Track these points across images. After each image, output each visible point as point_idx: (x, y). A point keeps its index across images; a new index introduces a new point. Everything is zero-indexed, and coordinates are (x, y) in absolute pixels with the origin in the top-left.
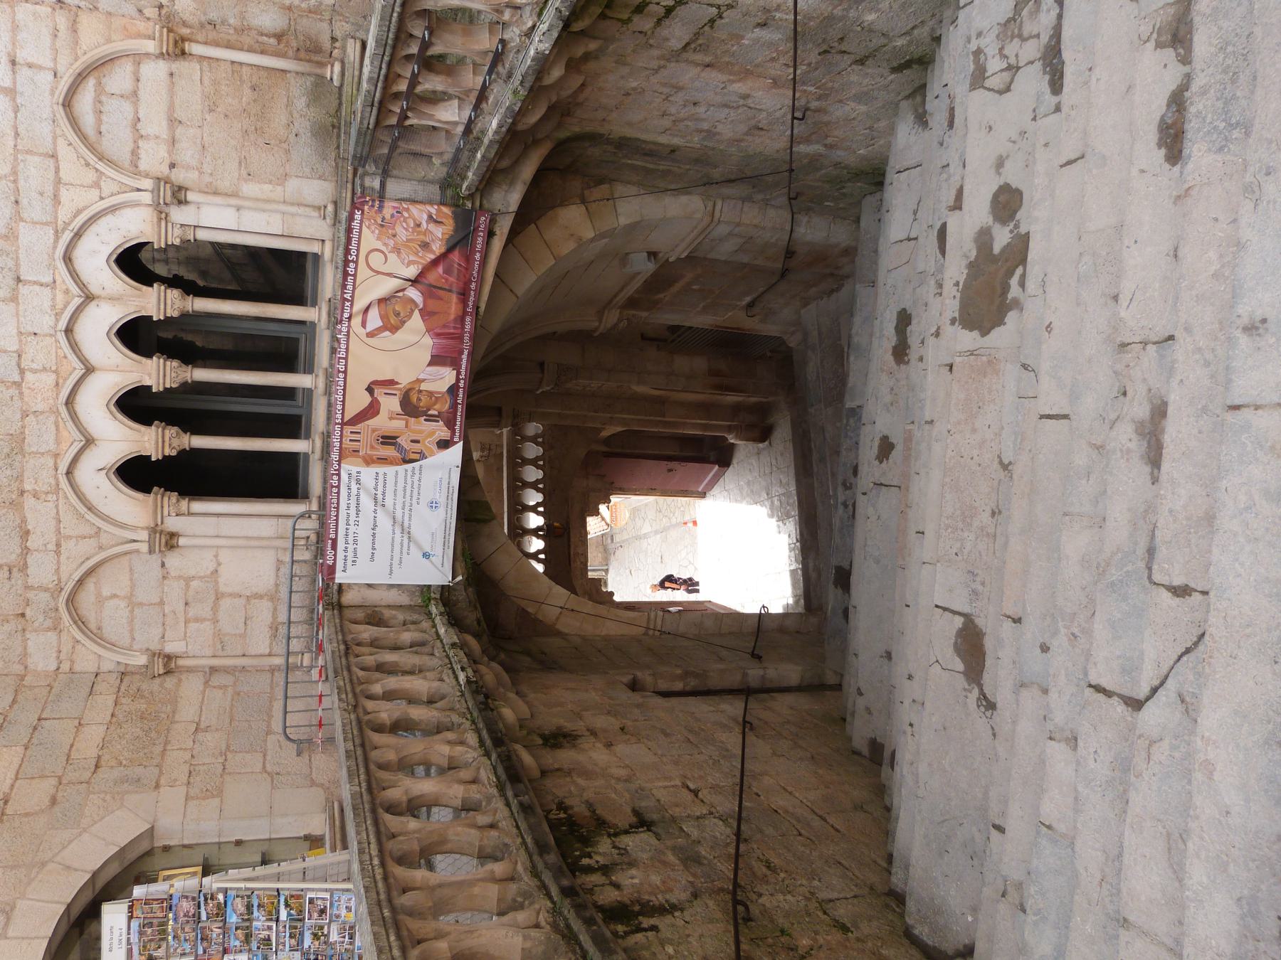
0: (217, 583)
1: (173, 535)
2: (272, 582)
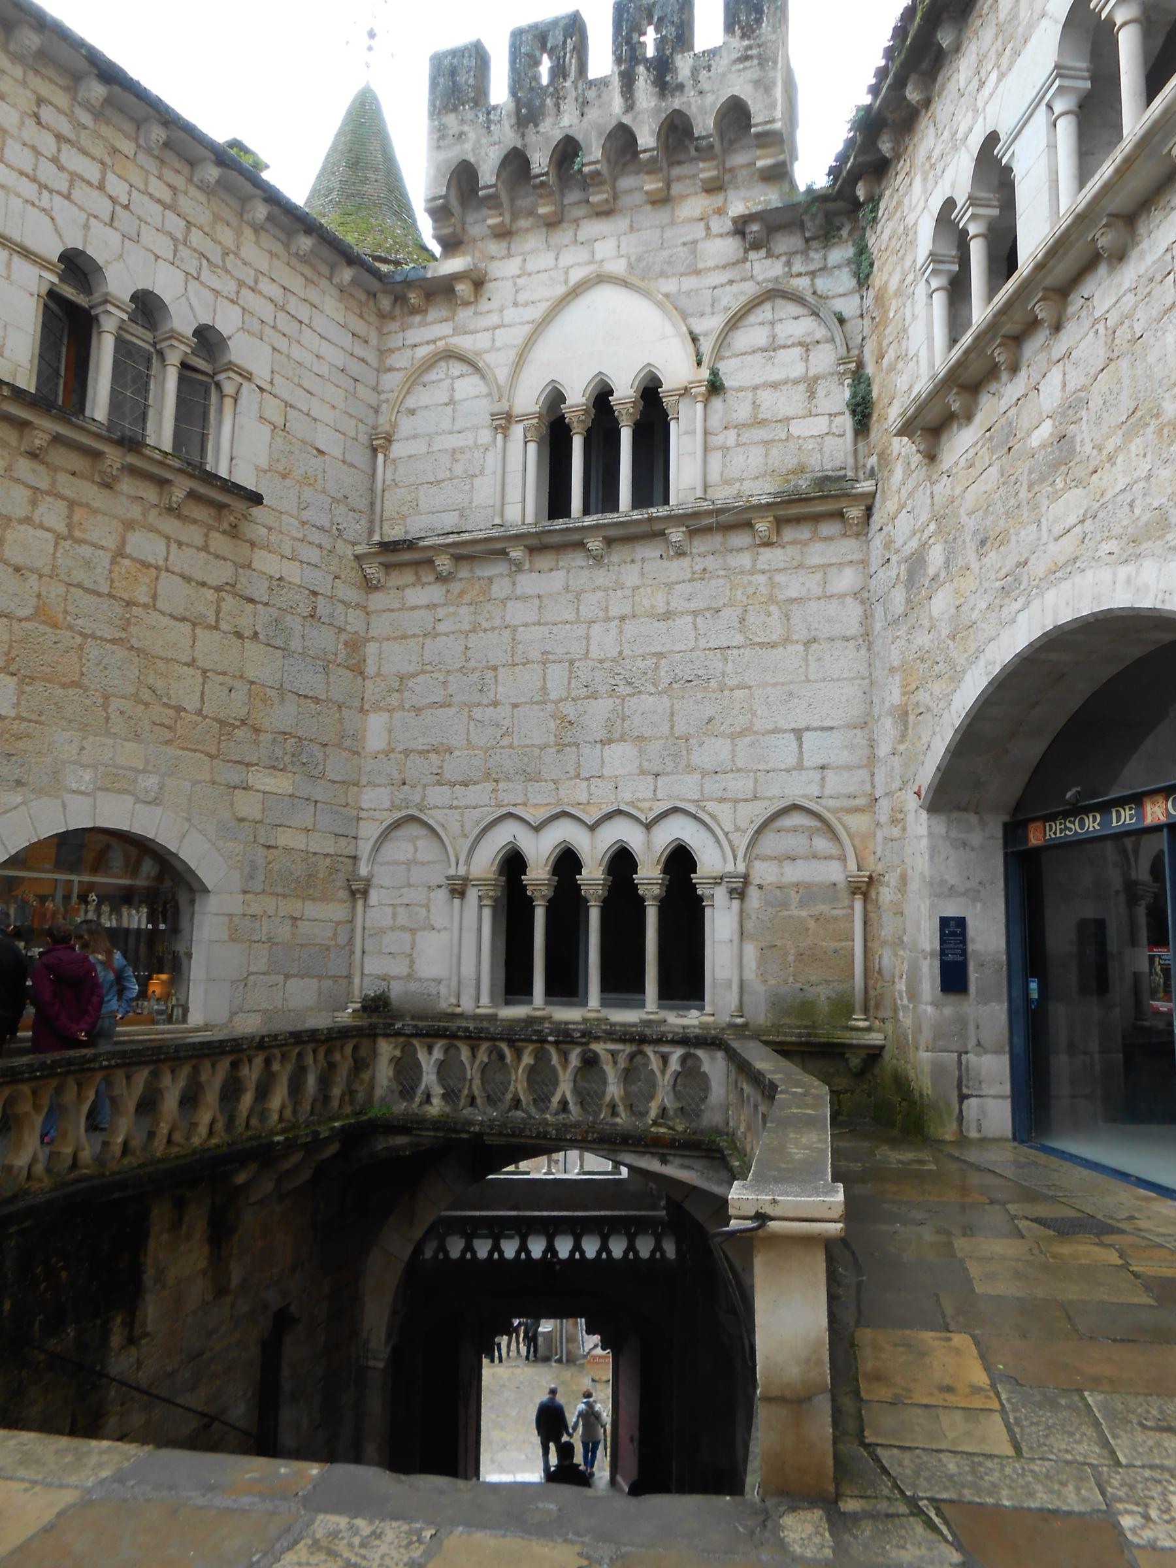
0: (424, 929)
1: (462, 894)
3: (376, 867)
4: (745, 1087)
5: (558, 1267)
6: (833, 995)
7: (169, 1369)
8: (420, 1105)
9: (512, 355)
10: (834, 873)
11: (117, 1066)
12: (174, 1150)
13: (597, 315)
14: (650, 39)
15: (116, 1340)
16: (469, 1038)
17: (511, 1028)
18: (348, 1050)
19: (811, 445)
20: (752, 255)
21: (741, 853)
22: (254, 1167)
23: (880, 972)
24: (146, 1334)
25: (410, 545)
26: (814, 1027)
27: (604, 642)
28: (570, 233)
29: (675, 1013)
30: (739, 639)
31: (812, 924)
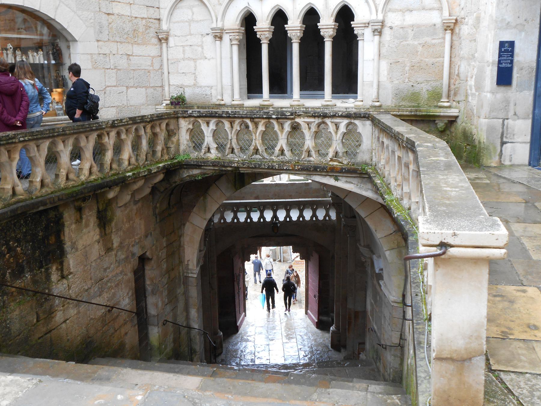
0: (201, 59)
1: (221, 38)
2: (203, 84)
3: (171, 25)
4: (385, 140)
5: (279, 225)
6: (430, 88)
7: (86, 288)
8: (205, 153)
11: (29, 140)
12: (71, 184)
15: (54, 277)
16: (229, 117)
17: (252, 112)
18: (164, 126)
21: (380, 8)
22: (117, 189)
23: (458, 75)
24: (71, 273)
26: (418, 107)
29: (340, 101)
31: (420, 49)
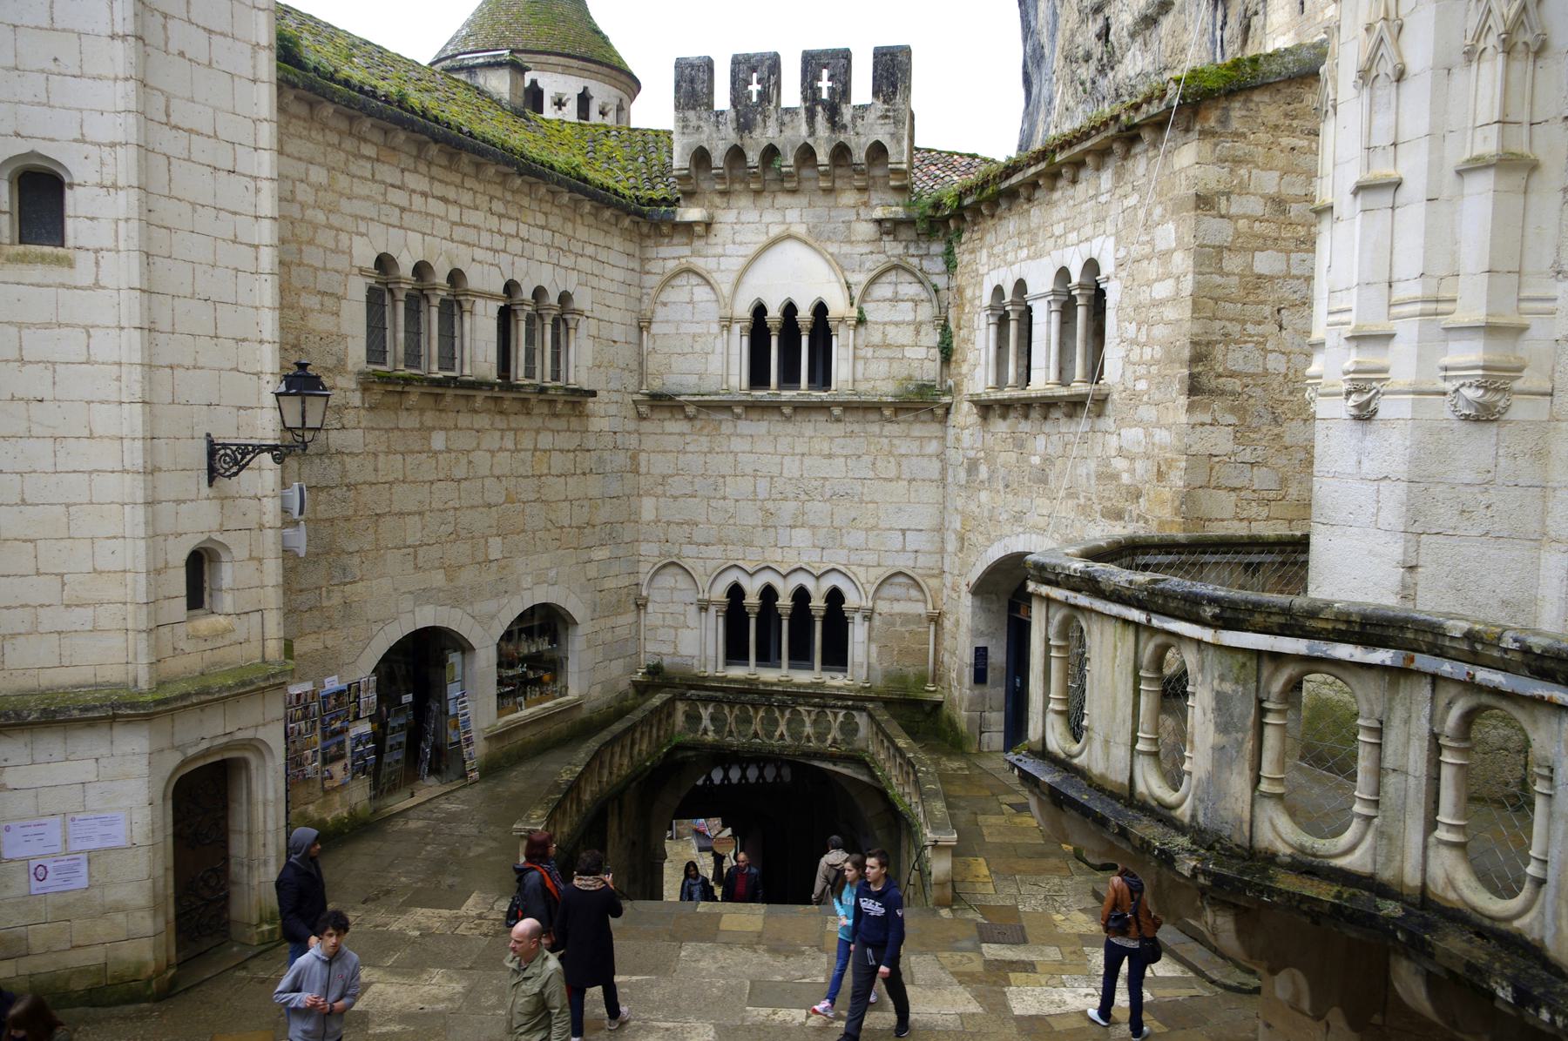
9: (733, 277)
10: (920, 609)
13: (787, 259)
14: (824, 84)
19: (916, 364)
20: (885, 238)
25: (670, 397)
27: (792, 467)
28: (770, 200)
30: (871, 474)
